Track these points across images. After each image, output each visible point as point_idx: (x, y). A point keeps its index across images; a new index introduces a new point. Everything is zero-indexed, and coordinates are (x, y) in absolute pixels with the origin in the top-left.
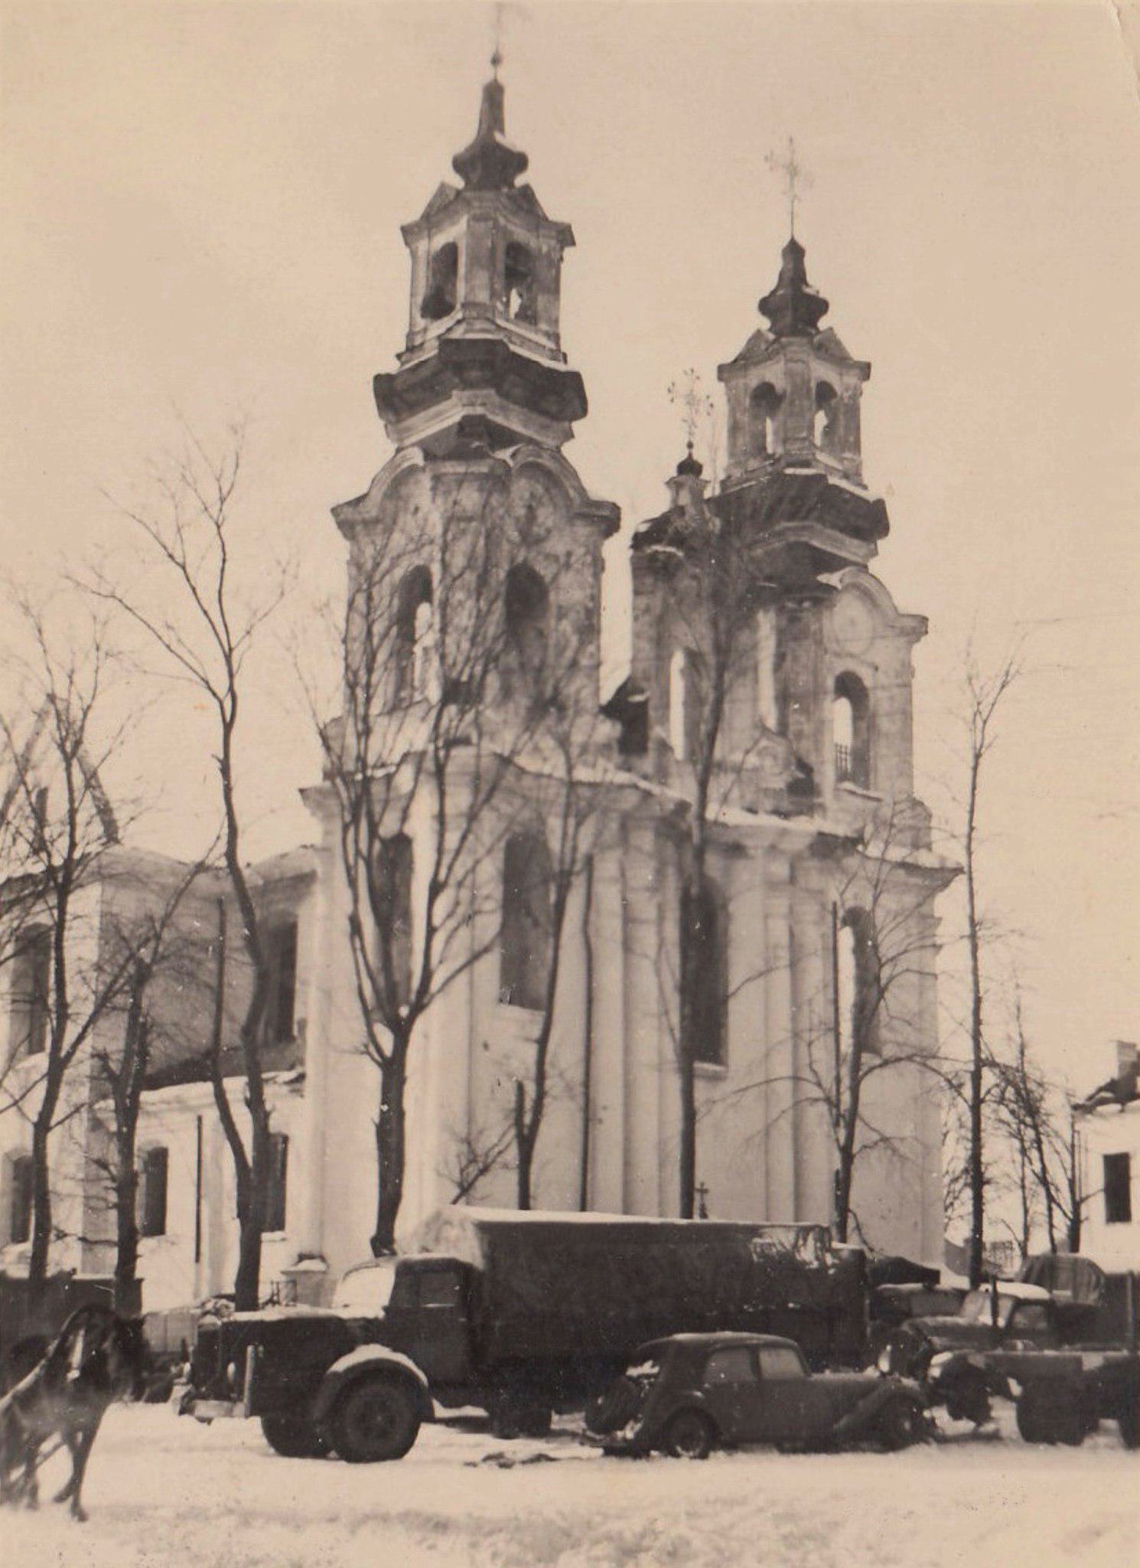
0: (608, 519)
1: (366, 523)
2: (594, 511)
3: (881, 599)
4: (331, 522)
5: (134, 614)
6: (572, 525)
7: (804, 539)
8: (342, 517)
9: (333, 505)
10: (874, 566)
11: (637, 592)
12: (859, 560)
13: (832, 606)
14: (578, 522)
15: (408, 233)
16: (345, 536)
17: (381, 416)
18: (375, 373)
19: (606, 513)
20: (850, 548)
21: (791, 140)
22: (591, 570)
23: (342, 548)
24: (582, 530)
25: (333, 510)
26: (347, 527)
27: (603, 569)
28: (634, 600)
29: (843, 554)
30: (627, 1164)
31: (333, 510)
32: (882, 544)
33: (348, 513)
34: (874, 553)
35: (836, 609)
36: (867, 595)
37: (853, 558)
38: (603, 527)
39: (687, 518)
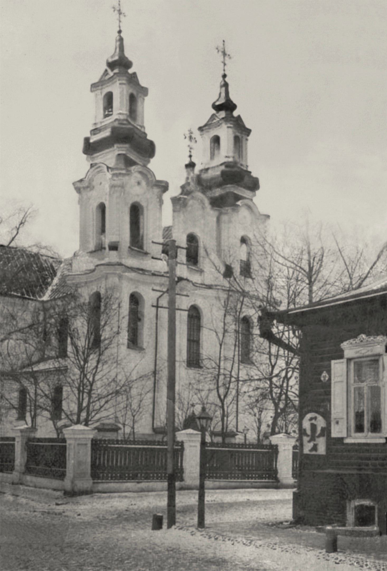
0: (164, 187)
1: (84, 188)
2: (160, 184)
3: (254, 209)
4: (72, 188)
5: (15, 236)
6: (153, 189)
7: (232, 190)
8: (76, 186)
9: (73, 182)
10: (255, 200)
11: (174, 211)
12: (250, 198)
13: (238, 212)
14: (155, 188)
15: (94, 86)
16: (77, 192)
17: (380, 411)
18: (170, 197)
19: (164, 184)
20: (246, 193)
21: (224, 41)
22: (159, 204)
23: (75, 195)
24: (156, 190)
25: (74, 184)
26: (78, 190)
27: (163, 203)
28: (173, 214)
29: (244, 195)
30: (231, 505)
31: (74, 184)
32: (257, 192)
33: (79, 185)
34: (255, 195)
35: (240, 213)
36: (249, 208)
37: (248, 197)
38: (163, 189)
39: (191, 186)
